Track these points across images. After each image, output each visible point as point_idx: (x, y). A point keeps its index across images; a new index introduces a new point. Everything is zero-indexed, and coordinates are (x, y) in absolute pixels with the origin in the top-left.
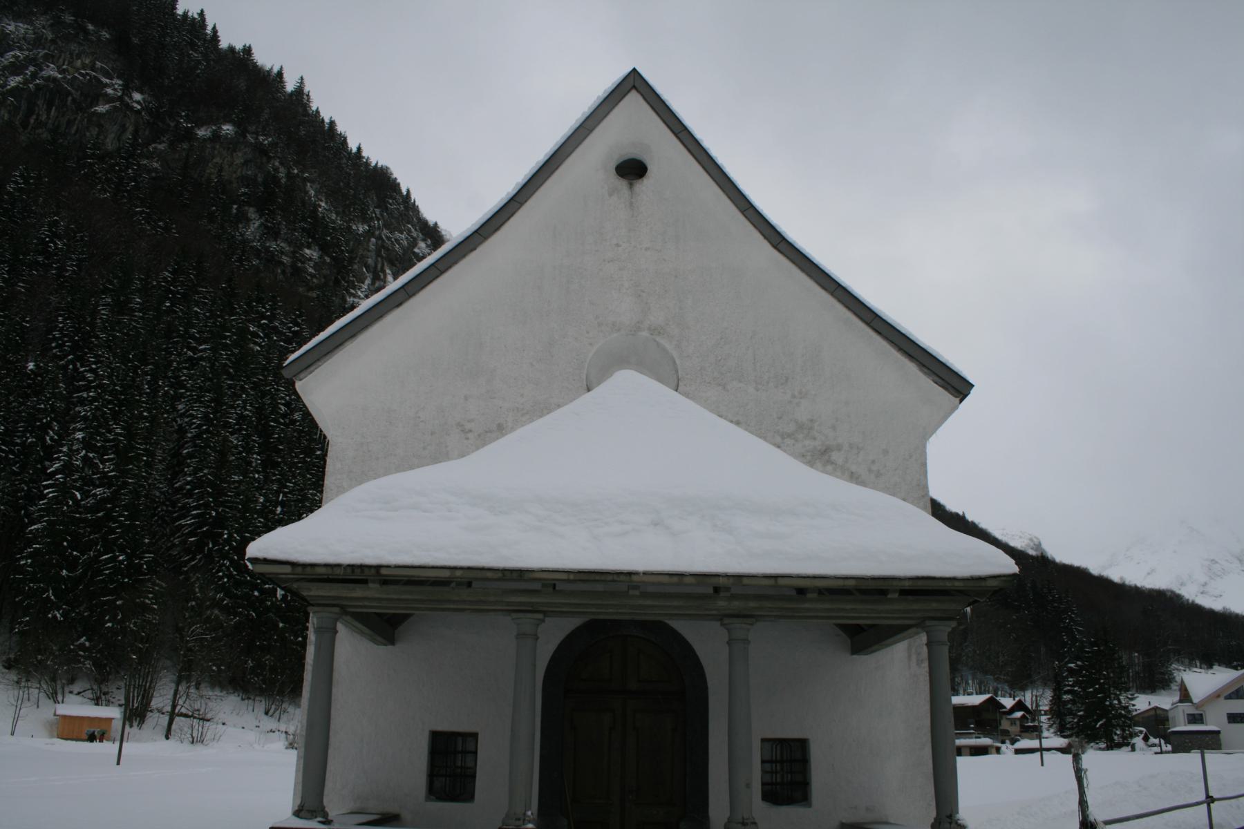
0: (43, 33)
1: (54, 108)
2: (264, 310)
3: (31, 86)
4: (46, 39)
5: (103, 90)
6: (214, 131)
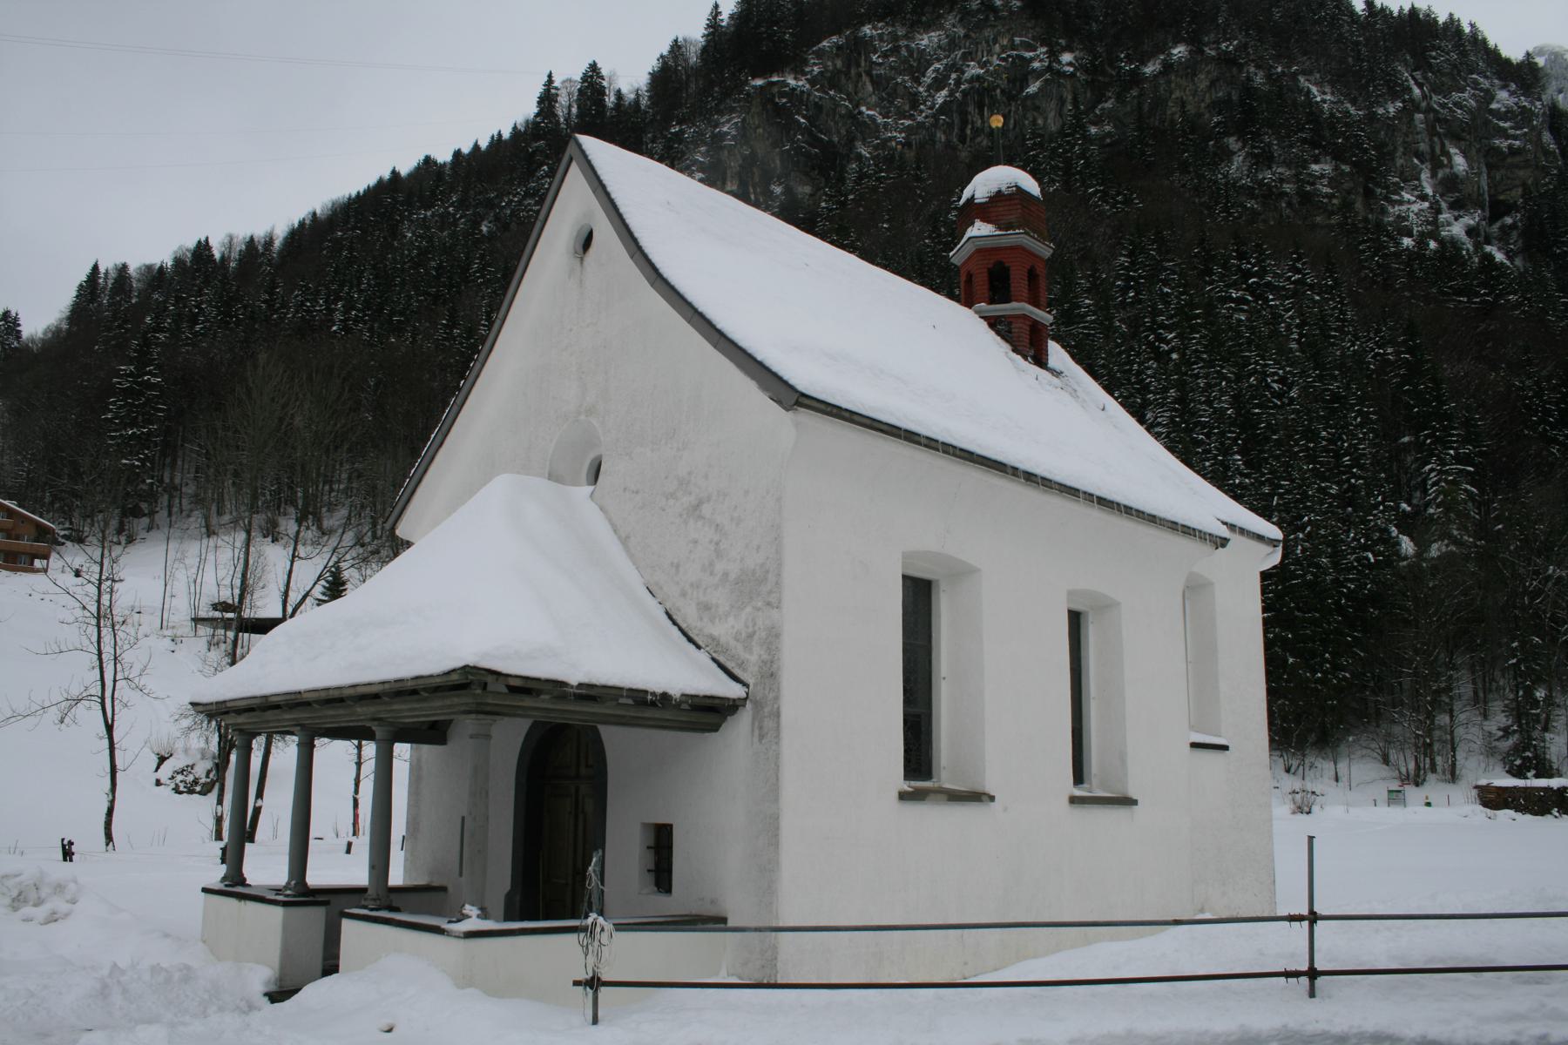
0: (954, 32)
1: (986, 109)
2: (1249, 266)
3: (957, 95)
4: (959, 37)
5: (1028, 66)
6: (1165, 60)
